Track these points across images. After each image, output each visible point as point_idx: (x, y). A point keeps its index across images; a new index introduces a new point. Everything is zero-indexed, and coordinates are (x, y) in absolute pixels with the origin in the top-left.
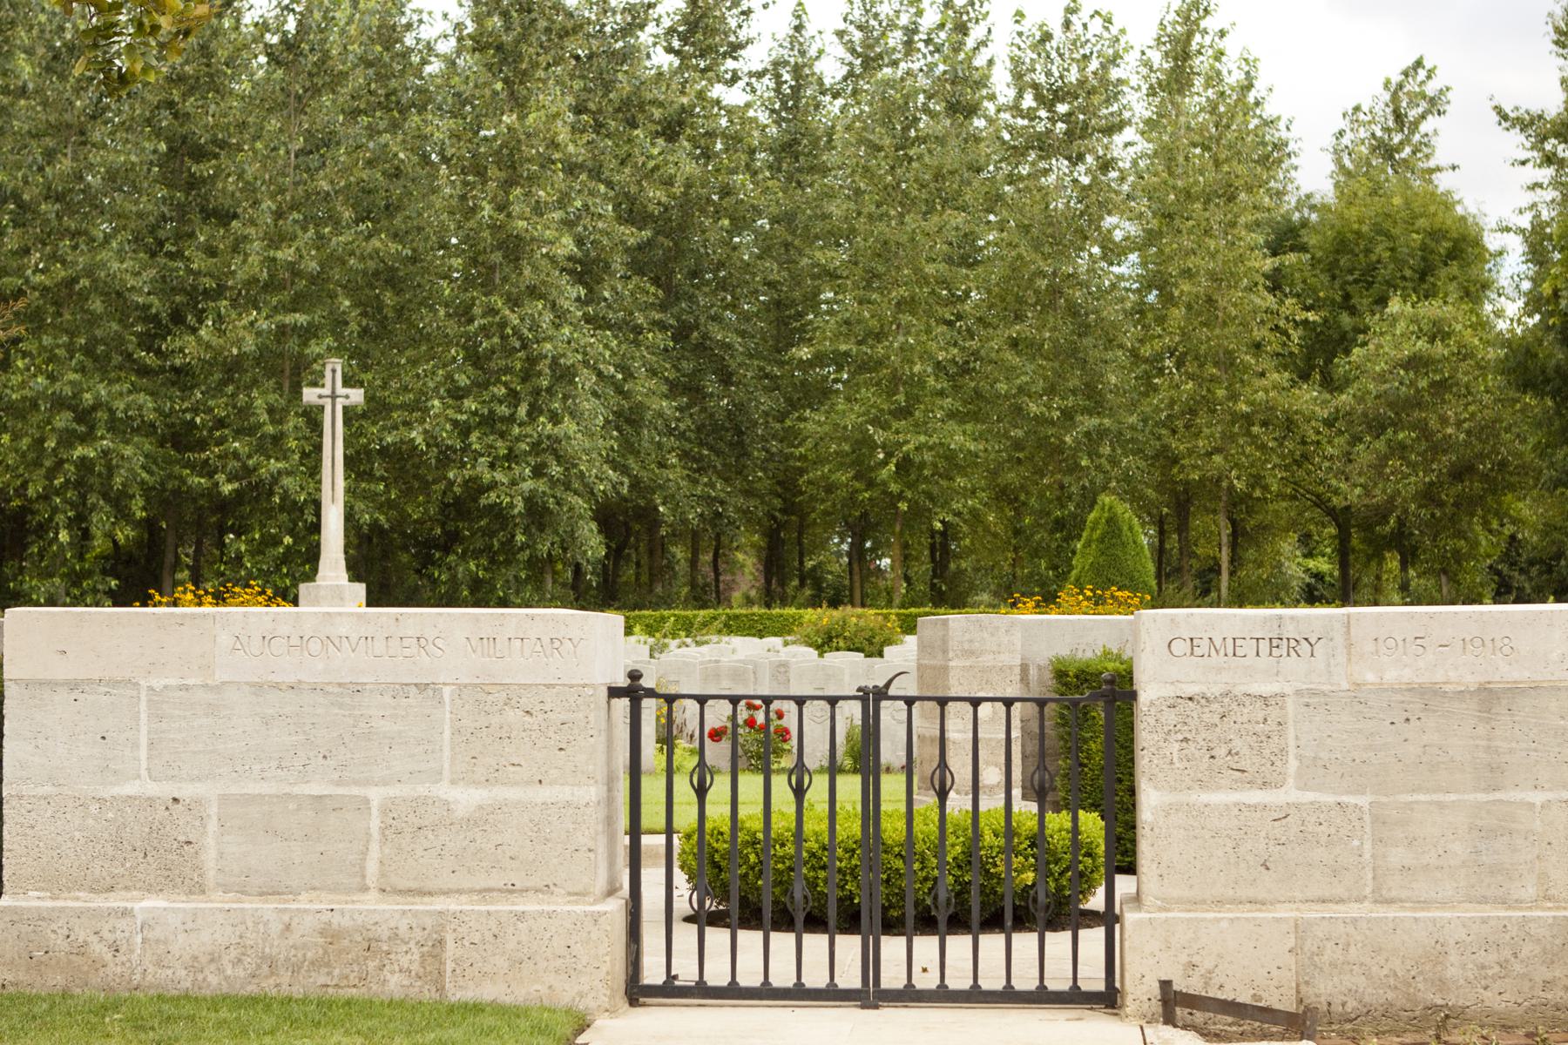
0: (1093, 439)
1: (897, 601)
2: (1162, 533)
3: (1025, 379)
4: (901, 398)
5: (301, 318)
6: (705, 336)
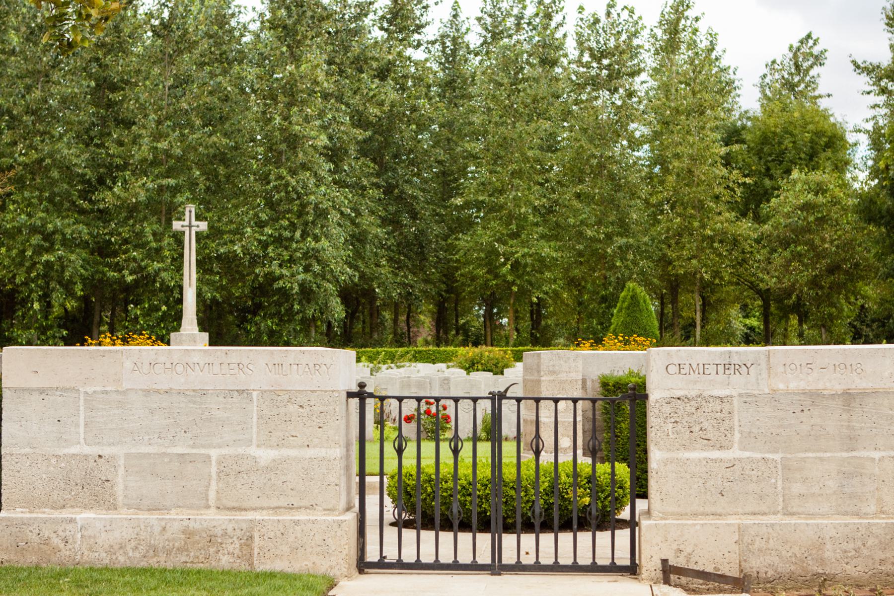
0: (623, 250)
1: (511, 343)
2: (662, 304)
3: (584, 216)
4: (514, 227)
5: (172, 182)
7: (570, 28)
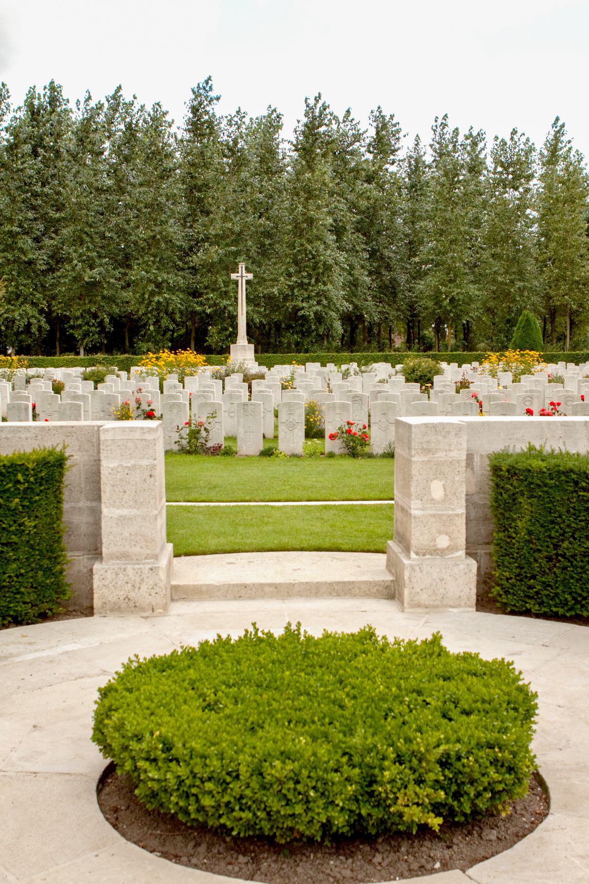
0: (521, 290)
1: (450, 348)
2: (545, 323)
3: (496, 268)
6: (382, 254)
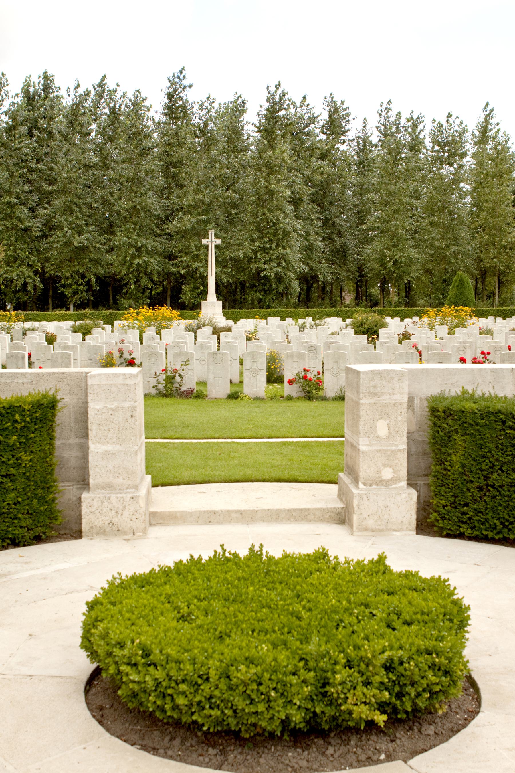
0: (456, 254)
1: (393, 305)
2: (477, 282)
3: (434, 235)
4: (395, 241)
5: (204, 217)
7: (427, 132)
